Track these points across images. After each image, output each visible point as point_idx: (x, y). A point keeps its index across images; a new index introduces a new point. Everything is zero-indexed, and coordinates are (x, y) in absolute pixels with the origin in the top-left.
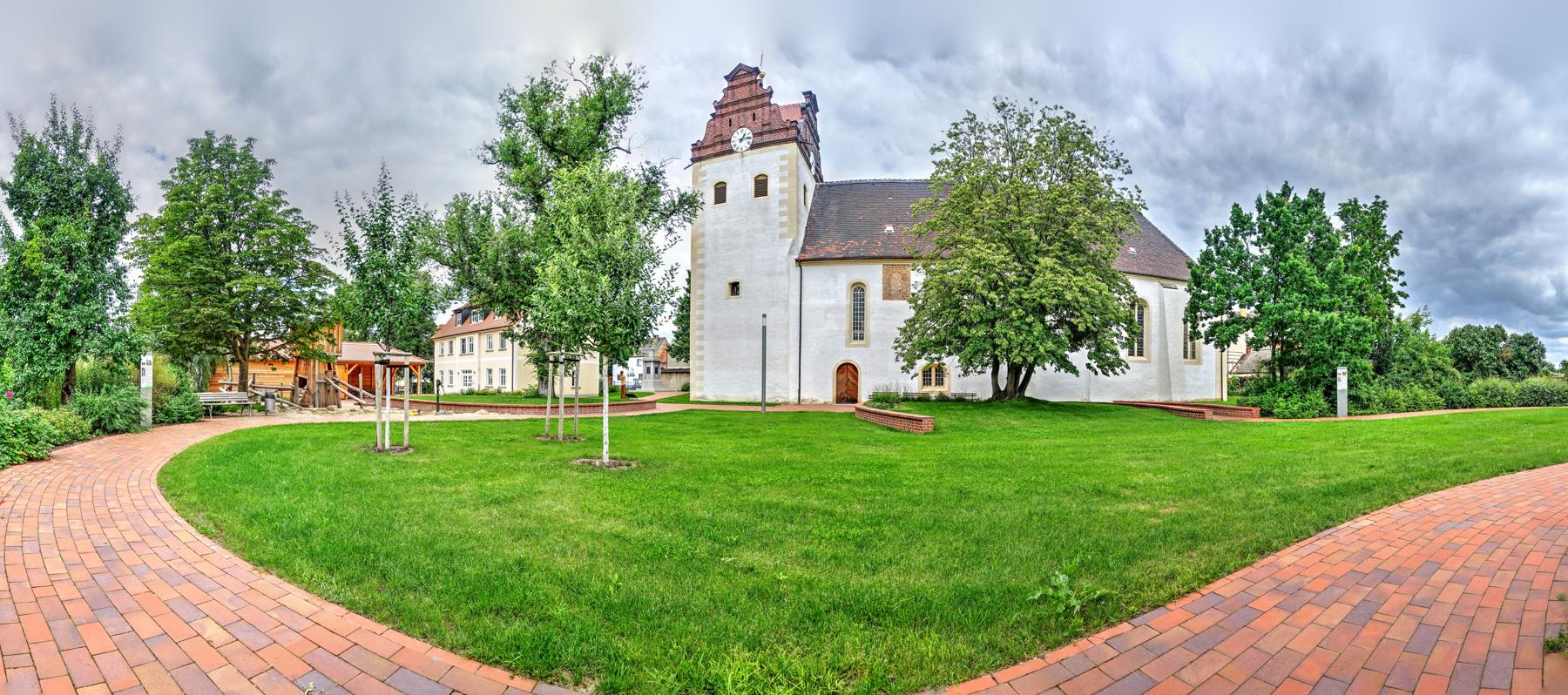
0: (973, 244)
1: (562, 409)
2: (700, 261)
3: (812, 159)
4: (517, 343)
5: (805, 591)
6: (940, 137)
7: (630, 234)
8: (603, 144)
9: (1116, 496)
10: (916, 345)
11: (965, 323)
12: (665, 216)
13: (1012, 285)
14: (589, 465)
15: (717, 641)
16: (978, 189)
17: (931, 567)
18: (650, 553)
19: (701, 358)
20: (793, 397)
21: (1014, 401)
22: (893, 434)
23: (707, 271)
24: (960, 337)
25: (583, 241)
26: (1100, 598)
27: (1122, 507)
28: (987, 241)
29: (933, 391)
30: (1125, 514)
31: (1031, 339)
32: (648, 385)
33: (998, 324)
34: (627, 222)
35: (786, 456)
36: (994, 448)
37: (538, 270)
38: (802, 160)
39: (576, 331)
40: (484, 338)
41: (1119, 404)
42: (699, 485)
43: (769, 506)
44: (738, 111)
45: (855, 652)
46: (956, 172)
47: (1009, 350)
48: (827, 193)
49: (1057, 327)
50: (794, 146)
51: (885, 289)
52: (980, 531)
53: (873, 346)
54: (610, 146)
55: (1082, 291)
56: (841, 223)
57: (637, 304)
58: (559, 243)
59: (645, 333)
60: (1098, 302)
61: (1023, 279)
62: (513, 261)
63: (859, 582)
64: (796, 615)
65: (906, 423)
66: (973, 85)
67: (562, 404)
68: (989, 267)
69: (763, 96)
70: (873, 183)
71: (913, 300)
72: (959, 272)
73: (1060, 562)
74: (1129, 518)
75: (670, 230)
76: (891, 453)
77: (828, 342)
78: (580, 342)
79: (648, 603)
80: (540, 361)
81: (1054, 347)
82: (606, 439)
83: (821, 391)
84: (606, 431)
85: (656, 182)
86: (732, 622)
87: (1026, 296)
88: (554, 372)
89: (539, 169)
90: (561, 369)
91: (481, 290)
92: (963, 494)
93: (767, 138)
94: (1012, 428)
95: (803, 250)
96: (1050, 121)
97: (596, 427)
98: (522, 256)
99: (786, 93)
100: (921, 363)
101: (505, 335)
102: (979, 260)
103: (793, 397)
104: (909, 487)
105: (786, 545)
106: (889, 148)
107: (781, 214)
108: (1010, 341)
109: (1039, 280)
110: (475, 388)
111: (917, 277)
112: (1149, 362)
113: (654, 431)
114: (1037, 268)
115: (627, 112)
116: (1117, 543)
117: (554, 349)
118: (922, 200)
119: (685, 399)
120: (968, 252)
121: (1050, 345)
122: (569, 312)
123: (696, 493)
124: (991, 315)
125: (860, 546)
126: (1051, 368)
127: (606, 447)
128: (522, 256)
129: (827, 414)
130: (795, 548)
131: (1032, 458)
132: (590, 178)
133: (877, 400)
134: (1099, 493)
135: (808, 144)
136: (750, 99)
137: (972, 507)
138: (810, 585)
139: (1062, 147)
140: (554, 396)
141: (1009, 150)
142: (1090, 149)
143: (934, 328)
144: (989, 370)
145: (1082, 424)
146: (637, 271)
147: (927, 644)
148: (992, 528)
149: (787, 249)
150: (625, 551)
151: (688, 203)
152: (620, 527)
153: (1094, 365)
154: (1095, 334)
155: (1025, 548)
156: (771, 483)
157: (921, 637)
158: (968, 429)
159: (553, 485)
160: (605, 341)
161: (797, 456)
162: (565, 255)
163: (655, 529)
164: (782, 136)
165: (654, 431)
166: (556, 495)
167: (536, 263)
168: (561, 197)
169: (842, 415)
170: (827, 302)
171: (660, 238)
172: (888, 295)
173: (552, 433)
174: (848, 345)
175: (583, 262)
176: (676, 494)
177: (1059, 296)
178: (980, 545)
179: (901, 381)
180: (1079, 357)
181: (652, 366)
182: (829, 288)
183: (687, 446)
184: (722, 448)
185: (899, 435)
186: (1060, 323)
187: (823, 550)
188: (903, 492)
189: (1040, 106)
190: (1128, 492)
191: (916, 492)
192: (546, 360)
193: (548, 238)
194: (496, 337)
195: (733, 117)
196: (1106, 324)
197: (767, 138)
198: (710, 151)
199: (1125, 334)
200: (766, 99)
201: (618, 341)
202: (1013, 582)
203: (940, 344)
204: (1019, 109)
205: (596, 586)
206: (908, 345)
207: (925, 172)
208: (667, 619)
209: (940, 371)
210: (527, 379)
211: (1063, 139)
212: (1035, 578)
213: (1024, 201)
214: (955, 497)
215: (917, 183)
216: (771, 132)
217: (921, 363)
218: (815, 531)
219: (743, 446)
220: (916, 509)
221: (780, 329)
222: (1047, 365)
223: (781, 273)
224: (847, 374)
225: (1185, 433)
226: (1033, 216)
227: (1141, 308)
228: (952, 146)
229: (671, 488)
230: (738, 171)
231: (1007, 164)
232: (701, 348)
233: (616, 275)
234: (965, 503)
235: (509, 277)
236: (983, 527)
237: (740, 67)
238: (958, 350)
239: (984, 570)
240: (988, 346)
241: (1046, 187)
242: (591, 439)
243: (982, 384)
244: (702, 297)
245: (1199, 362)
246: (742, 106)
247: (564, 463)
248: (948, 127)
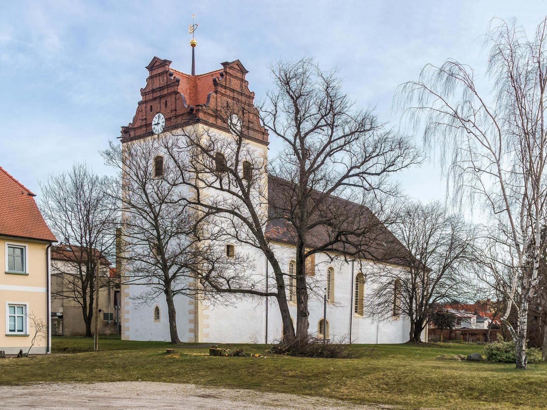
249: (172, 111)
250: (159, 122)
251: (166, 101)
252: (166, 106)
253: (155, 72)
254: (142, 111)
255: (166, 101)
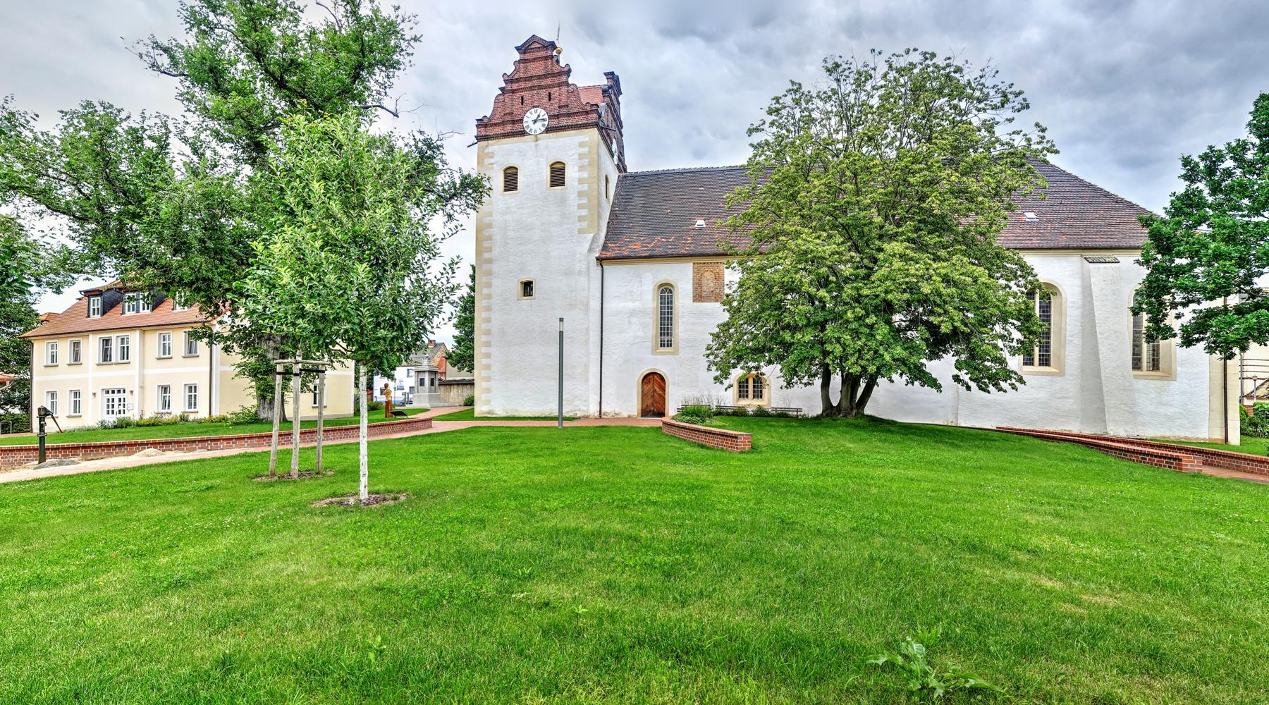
0: (798, 234)
1: (297, 436)
2: (486, 255)
3: (614, 147)
4: (218, 348)
5: (606, 624)
6: (758, 115)
7: (398, 217)
8: (358, 97)
9: (1002, 558)
10: (730, 352)
11: (788, 327)
12: (444, 199)
13: (847, 280)
14: (339, 505)
15: (507, 690)
16: (804, 170)
17: (748, 603)
18: (424, 601)
19: (488, 367)
20: (593, 410)
21: (850, 420)
22: (704, 452)
23: (495, 267)
24: (783, 343)
25: (329, 216)
26: (974, 691)
27: (1012, 575)
28: (815, 229)
29: (751, 404)
30: (1017, 586)
31: (872, 344)
32: (421, 400)
33: (829, 327)
34: (393, 201)
35: (586, 476)
36: (825, 474)
37: (258, 246)
38: (603, 148)
39: (320, 332)
40: (153, 339)
41: (1007, 434)
42: (485, 514)
43: (567, 532)
44: (531, 88)
45: (662, 693)
46: (778, 153)
47: (843, 358)
48: (630, 184)
49: (909, 328)
50: (595, 131)
51: (695, 290)
52: (806, 570)
53: (682, 354)
54: (370, 102)
55: (947, 280)
56: (646, 218)
57: (407, 302)
58: (292, 213)
59: (417, 337)
60: (972, 293)
61: (862, 272)
62: (212, 228)
63: (667, 615)
64: (597, 651)
65: (719, 440)
66: (798, 50)
67: (297, 429)
68: (818, 260)
69: (560, 74)
70: (682, 173)
71: (727, 302)
72: (781, 267)
73: (913, 625)
74: (1024, 593)
75: (450, 216)
76: (702, 473)
77: (633, 350)
78: (326, 347)
79: (421, 663)
80: (261, 373)
81: (905, 354)
82: (364, 469)
83: (624, 403)
84: (364, 459)
85: (431, 158)
86: (524, 666)
87: (865, 292)
88: (285, 387)
89: (258, 106)
90: (295, 382)
91: (144, 264)
92: (786, 524)
93: (564, 121)
94: (848, 451)
95: (605, 247)
96: (899, 71)
97: (350, 456)
98: (229, 223)
99: (586, 73)
100: (737, 373)
101: (195, 335)
102: (806, 252)
104: (723, 512)
105: (586, 574)
106: (700, 133)
107: (580, 207)
108: (844, 347)
109: (884, 271)
110: (133, 415)
111: (732, 276)
112: (1061, 374)
113: (429, 455)
114: (881, 256)
115: (395, 65)
116: (1004, 624)
117: (284, 355)
118: (737, 189)
119: (469, 415)
120: (792, 244)
121: (899, 351)
122: (308, 307)
123: (482, 522)
124: (820, 316)
125: (667, 575)
126: (900, 380)
127: (364, 480)
128: (229, 223)
129: (631, 429)
130: (596, 577)
131: (874, 490)
132: (340, 136)
133: (687, 414)
134: (973, 548)
135: (610, 130)
136: (545, 76)
137: (797, 541)
138: (612, 617)
139: (916, 100)
140: (284, 420)
141: (843, 117)
143: (751, 333)
144: (818, 382)
145: (946, 454)
146: (406, 262)
147: (743, 691)
148: (821, 567)
149: (587, 245)
150: (389, 605)
151: (471, 188)
152: (383, 577)
153: (966, 378)
154: (967, 337)
155: (864, 599)
156: (570, 507)
157: (737, 681)
158: (792, 450)
159: (287, 538)
160: (362, 346)
161: (598, 475)
162: (303, 231)
163: (431, 572)
164: (581, 120)
165: (429, 455)
166: (285, 554)
167: (254, 236)
168: (296, 152)
169: (647, 430)
170: (630, 305)
171: (436, 225)
172: (699, 297)
173: (280, 471)
174: (654, 352)
175: (329, 243)
176: (458, 526)
177: (911, 289)
178: (806, 587)
179: (714, 393)
180: (943, 367)
181: (427, 378)
182: (634, 289)
183: (472, 469)
184: (513, 470)
185: (711, 453)
186: (914, 323)
187: (626, 579)
188: (716, 517)
189: (885, 56)
190: (1023, 557)
191: (731, 517)
192: (271, 371)
193: (273, 203)
194: (178, 340)
196: (985, 322)
197: (564, 121)
198: (498, 130)
199: (1017, 335)
200: (563, 78)
201: (382, 346)
202: (848, 637)
203: (759, 351)
204: (857, 65)
205: (350, 657)
206: (722, 353)
207: (741, 157)
208: (446, 675)
209: (759, 382)
210: (244, 397)
211: (917, 89)
212: (878, 638)
213: (863, 177)
214: (776, 526)
215: (732, 170)
216: (568, 115)
217: (737, 373)
218: (618, 559)
219: (537, 466)
220: (731, 537)
221: (573, 333)
222: (895, 376)
223: (580, 273)
224: (654, 384)
225: (1134, 486)
226: (877, 192)
227: (1046, 298)
228: (772, 124)
229: (451, 521)
230: (532, 153)
231: (841, 136)
232: (488, 356)
233: (378, 265)
234: (789, 535)
235: (204, 251)
236: (810, 566)
237: (534, 39)
238: (780, 358)
239: (812, 615)
240: (816, 353)
241: (893, 154)
242: (343, 472)
243: (809, 398)
244: (489, 297)
245: (1170, 376)
246: (536, 83)
247: (301, 508)
248: (768, 103)
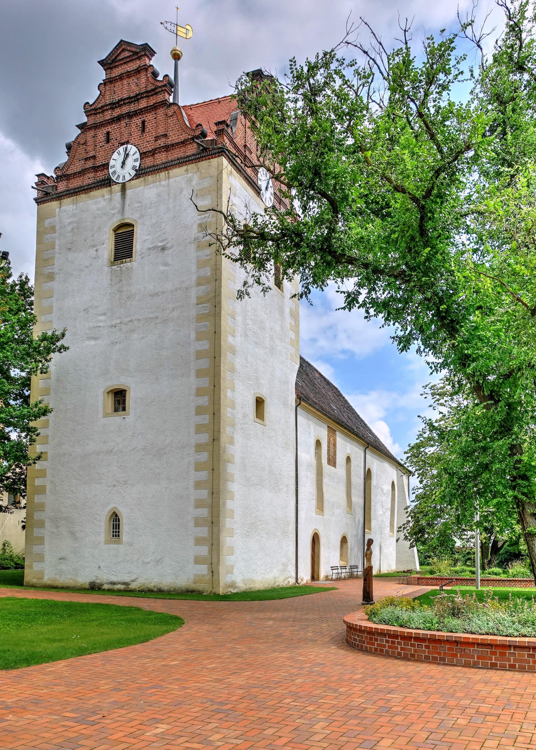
103: (292, 581)
142: (382, 306)
195: (149, 117)
197: (161, 158)
216: (167, 148)
246: (125, 109)
249: (157, 138)
250: (123, 162)
251: (143, 122)
252: (143, 130)
253: (117, 72)
254: (85, 143)
255: (143, 122)
